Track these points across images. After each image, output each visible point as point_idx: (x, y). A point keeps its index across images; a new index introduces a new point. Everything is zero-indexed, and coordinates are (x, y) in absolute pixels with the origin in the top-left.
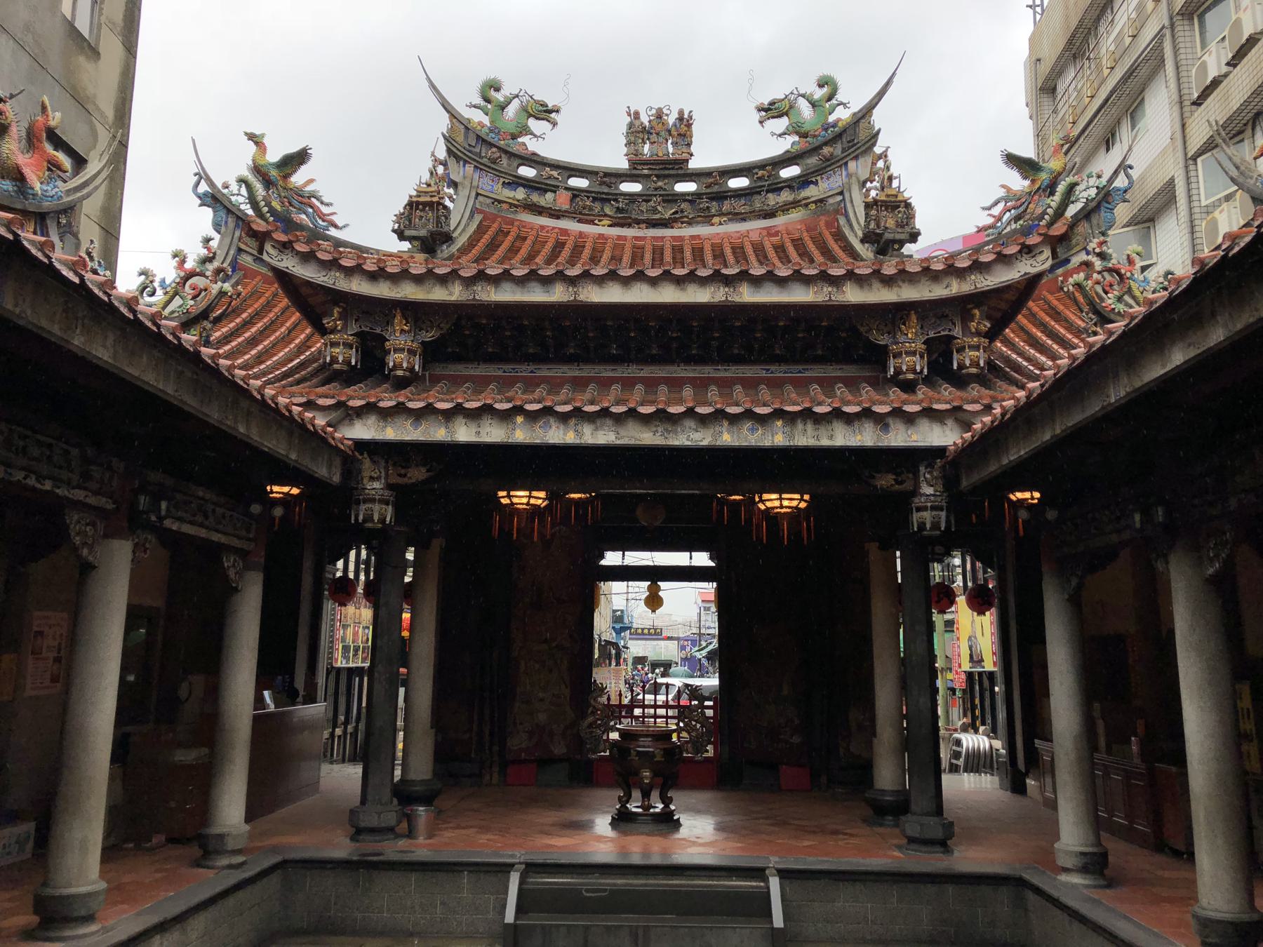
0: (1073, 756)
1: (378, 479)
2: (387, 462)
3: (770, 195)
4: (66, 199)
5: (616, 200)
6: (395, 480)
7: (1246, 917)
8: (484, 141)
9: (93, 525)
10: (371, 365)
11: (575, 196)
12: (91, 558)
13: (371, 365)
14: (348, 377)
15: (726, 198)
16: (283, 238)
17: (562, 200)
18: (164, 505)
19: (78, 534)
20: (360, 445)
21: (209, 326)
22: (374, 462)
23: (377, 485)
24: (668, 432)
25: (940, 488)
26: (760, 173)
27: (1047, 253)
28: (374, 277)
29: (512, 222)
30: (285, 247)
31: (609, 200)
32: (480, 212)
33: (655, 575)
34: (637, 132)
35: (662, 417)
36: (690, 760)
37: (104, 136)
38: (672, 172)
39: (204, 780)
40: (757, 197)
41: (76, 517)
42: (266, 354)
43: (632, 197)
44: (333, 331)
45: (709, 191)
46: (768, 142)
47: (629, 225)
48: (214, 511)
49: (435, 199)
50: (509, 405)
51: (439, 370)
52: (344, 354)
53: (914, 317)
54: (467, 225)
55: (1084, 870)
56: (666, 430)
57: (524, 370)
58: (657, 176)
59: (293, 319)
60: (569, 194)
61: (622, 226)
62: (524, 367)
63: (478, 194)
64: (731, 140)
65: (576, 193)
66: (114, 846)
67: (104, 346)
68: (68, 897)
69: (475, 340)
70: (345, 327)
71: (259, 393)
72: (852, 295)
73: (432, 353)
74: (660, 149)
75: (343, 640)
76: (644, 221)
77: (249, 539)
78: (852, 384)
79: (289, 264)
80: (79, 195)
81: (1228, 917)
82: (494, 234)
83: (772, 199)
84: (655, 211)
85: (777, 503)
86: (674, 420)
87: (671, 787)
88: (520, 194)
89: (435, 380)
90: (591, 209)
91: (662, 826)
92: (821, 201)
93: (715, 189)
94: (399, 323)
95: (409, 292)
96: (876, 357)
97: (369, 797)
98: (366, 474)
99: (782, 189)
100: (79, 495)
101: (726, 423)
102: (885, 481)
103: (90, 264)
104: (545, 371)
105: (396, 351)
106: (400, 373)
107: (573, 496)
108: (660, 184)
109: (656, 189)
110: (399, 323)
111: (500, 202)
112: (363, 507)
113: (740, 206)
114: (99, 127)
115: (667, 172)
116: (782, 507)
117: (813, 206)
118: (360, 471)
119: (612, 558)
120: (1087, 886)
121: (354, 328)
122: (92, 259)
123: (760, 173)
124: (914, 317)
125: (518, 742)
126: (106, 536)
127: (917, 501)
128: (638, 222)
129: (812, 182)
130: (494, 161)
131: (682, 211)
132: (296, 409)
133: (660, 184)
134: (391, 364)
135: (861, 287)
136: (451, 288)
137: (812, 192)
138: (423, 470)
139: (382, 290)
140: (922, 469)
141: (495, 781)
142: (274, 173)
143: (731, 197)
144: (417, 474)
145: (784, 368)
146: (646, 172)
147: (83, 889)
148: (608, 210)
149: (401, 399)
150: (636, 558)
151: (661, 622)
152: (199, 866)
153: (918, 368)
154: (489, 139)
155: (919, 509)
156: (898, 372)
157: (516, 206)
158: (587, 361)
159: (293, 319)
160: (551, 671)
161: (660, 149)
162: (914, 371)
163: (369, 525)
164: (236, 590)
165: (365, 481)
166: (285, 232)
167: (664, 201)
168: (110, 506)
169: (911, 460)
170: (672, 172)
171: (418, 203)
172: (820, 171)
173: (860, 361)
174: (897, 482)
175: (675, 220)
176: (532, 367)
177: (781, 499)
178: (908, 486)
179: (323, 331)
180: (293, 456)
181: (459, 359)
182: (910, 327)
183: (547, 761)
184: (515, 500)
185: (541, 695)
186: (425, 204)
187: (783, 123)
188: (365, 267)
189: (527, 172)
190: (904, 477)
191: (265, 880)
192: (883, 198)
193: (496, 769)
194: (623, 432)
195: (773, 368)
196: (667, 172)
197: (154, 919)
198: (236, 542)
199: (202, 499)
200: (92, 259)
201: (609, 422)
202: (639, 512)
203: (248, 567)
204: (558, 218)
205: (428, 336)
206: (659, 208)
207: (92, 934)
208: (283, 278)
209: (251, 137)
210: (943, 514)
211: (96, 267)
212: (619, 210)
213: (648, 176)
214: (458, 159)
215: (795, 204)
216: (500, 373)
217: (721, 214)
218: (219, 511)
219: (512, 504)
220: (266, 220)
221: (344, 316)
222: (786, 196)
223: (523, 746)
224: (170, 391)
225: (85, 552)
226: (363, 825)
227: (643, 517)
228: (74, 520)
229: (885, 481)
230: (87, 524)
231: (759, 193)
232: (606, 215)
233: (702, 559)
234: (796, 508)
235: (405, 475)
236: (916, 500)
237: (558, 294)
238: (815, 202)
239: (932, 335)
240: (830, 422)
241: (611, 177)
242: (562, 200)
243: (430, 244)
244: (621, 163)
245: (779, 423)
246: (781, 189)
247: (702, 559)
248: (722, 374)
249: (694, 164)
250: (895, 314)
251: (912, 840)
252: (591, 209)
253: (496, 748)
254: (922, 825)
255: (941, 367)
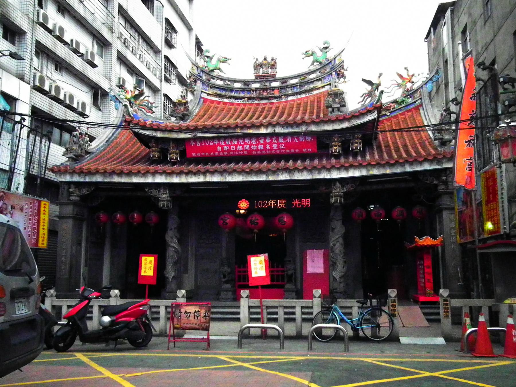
12: (169, 78)
13: (163, 159)
27: (376, 112)
34: (257, 66)
44: (153, 147)
46: (305, 66)
52: (155, 155)
64: (291, 66)
74: (265, 70)
94: (172, 145)
99: (313, 81)
102: (323, 189)
107: (370, 181)
110: (172, 145)
161: (265, 70)
179: (149, 147)
187: (311, 59)
189: (220, 83)
241: (246, 83)
244: (253, 77)
249: (278, 76)
255: (346, 151)
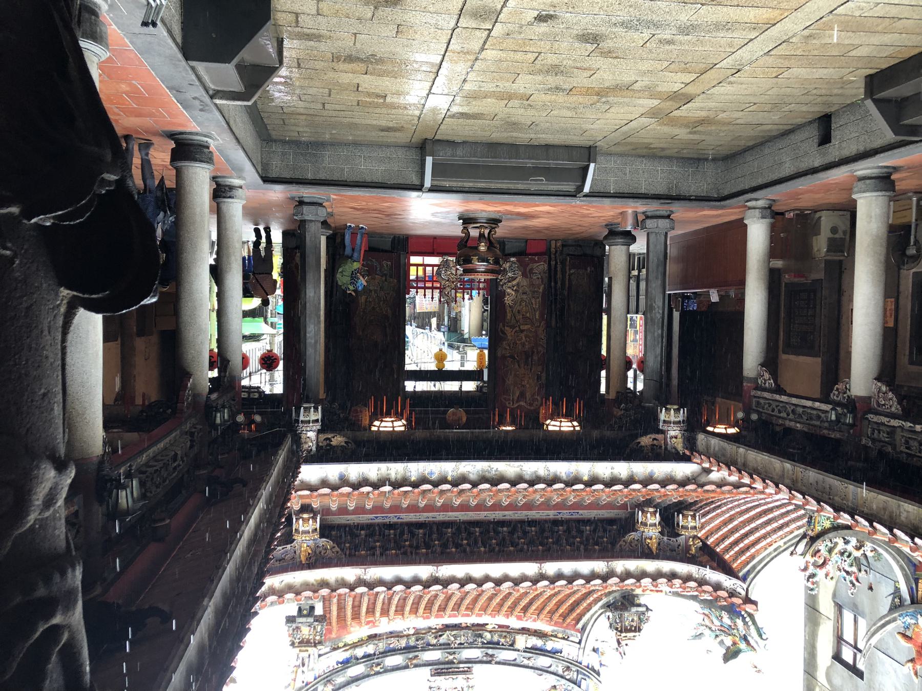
0: (233, 258)
1: (672, 437)
2: (666, 448)
3: (372, 652)
4: (896, 615)
5: (483, 643)
6: (660, 437)
7: (186, 163)
8: (575, 684)
9: (879, 405)
10: (669, 515)
11: (512, 645)
12: (879, 384)
14: (682, 507)
15: (405, 648)
16: (735, 600)
17: (522, 642)
18: (833, 417)
19: (891, 399)
20: (687, 459)
21: (810, 532)
22: (675, 448)
23: (672, 433)
24: (487, 471)
25: (303, 436)
26: (378, 669)
28: (672, 576)
29: (556, 624)
30: (732, 594)
31: (489, 643)
32: (578, 631)
33: (441, 375)
35: (496, 481)
36: (450, 255)
37: (821, 675)
38: (443, 666)
39: (775, 248)
40: (381, 650)
41: (893, 409)
42: (725, 523)
43: (471, 646)
45: (417, 653)
47: (473, 625)
48: (788, 415)
49: (623, 634)
50: (574, 487)
51: (621, 514)
53: (303, 559)
54: (589, 620)
55: (231, 188)
56: (489, 472)
57: (565, 514)
58: (454, 663)
59: (722, 546)
60: (517, 646)
61: (478, 625)
62: (565, 516)
63: (580, 643)
65: (512, 646)
66: (816, 212)
67: (908, 512)
68: (878, 191)
69: (602, 534)
70: (687, 541)
71: (780, 489)
72: (350, 573)
73: (629, 523)
75: (636, 332)
76: (463, 628)
77: (755, 397)
78: (343, 510)
79: (728, 582)
80: (887, 619)
81: (197, 164)
82: (571, 614)
83: (370, 649)
84: (455, 637)
85: (396, 424)
86: (484, 479)
87: (462, 239)
88: (550, 645)
89: (624, 506)
90: (500, 636)
91: (472, 216)
92: (334, 649)
93: (411, 655)
95: (650, 566)
96: (326, 530)
97: (663, 237)
98: (680, 440)
100: (895, 423)
101: (449, 478)
102: (338, 440)
103: (853, 578)
104: (551, 514)
105: (655, 525)
106: (651, 510)
107: (504, 428)
108: (451, 657)
109: (454, 653)
111: (564, 638)
112: (681, 419)
113: (395, 643)
114: (825, 683)
115: (446, 666)
116: (392, 422)
117: (341, 645)
118: (684, 443)
119: (469, 386)
120: (231, 177)
121: (681, 540)
122: (851, 582)
123: (378, 669)
124: (303, 559)
125: (540, 267)
126: (870, 398)
127: (318, 426)
128: (467, 627)
129: (341, 663)
130: (568, 668)
131: (436, 638)
132: (746, 480)
133: (451, 657)
134: (658, 515)
135: (343, 579)
136: (623, 569)
137: (341, 655)
138: (642, 444)
139: (667, 566)
140: (314, 449)
141: (553, 243)
142: (742, 645)
143: (401, 649)
144: (646, 441)
145: (387, 520)
146: (462, 665)
147: (867, 194)
148: (488, 636)
149: (663, 490)
150: (451, 386)
151: (439, 347)
152: (774, 201)
153: (301, 521)
154: (572, 685)
155: (317, 421)
156: (314, 518)
157: (552, 636)
158: (522, 522)
159: (722, 546)
160: (519, 312)
162: (303, 519)
163: (676, 407)
164: (762, 365)
165: (680, 436)
166: (733, 604)
167: (449, 644)
168: (870, 416)
169: (324, 455)
170: (443, 666)
171: (635, 631)
172: (335, 672)
173: (339, 527)
174: (329, 439)
175: (440, 630)
176: (559, 517)
177: (393, 427)
178: (322, 437)
180: (742, 450)
181: (611, 521)
182: (305, 551)
183: (520, 254)
184: (570, 424)
185: (525, 297)
186: (630, 631)
188: (680, 581)
190: (325, 443)
191: (734, 190)
192: (309, 649)
193: (553, 250)
194: (518, 470)
195: (395, 520)
196: (446, 666)
197: (821, 175)
198: (766, 395)
199: (797, 422)
200: (851, 582)
201: (527, 477)
202: (464, 419)
203: (755, 380)
204: (523, 629)
205: (633, 535)
206: (452, 639)
207: (862, 169)
208: (729, 571)
209: (759, 671)
210: (302, 418)
211: (848, 577)
212: (481, 636)
213: (460, 662)
214: (593, 669)
215: (355, 646)
216: (581, 512)
217: (408, 636)
218: (784, 415)
219: (571, 421)
220: (746, 612)
221: (688, 548)
222: (360, 652)
223: (536, 265)
224: (851, 487)
225: (884, 388)
226: (667, 220)
227: (461, 414)
228: (895, 408)
229: (338, 440)
230: (884, 405)
231: (381, 653)
232: (490, 632)
233: (410, 386)
234: (382, 421)
235: (654, 439)
236: (319, 427)
237: (551, 568)
238: (338, 648)
239: (288, 546)
240: (379, 480)
242: (522, 642)
243: (626, 601)
245: (413, 479)
246: (364, 657)
247: (410, 386)
248: (430, 514)
250: (316, 561)
251: (321, 205)
252: (500, 636)
253: (553, 263)
254: (317, 214)
